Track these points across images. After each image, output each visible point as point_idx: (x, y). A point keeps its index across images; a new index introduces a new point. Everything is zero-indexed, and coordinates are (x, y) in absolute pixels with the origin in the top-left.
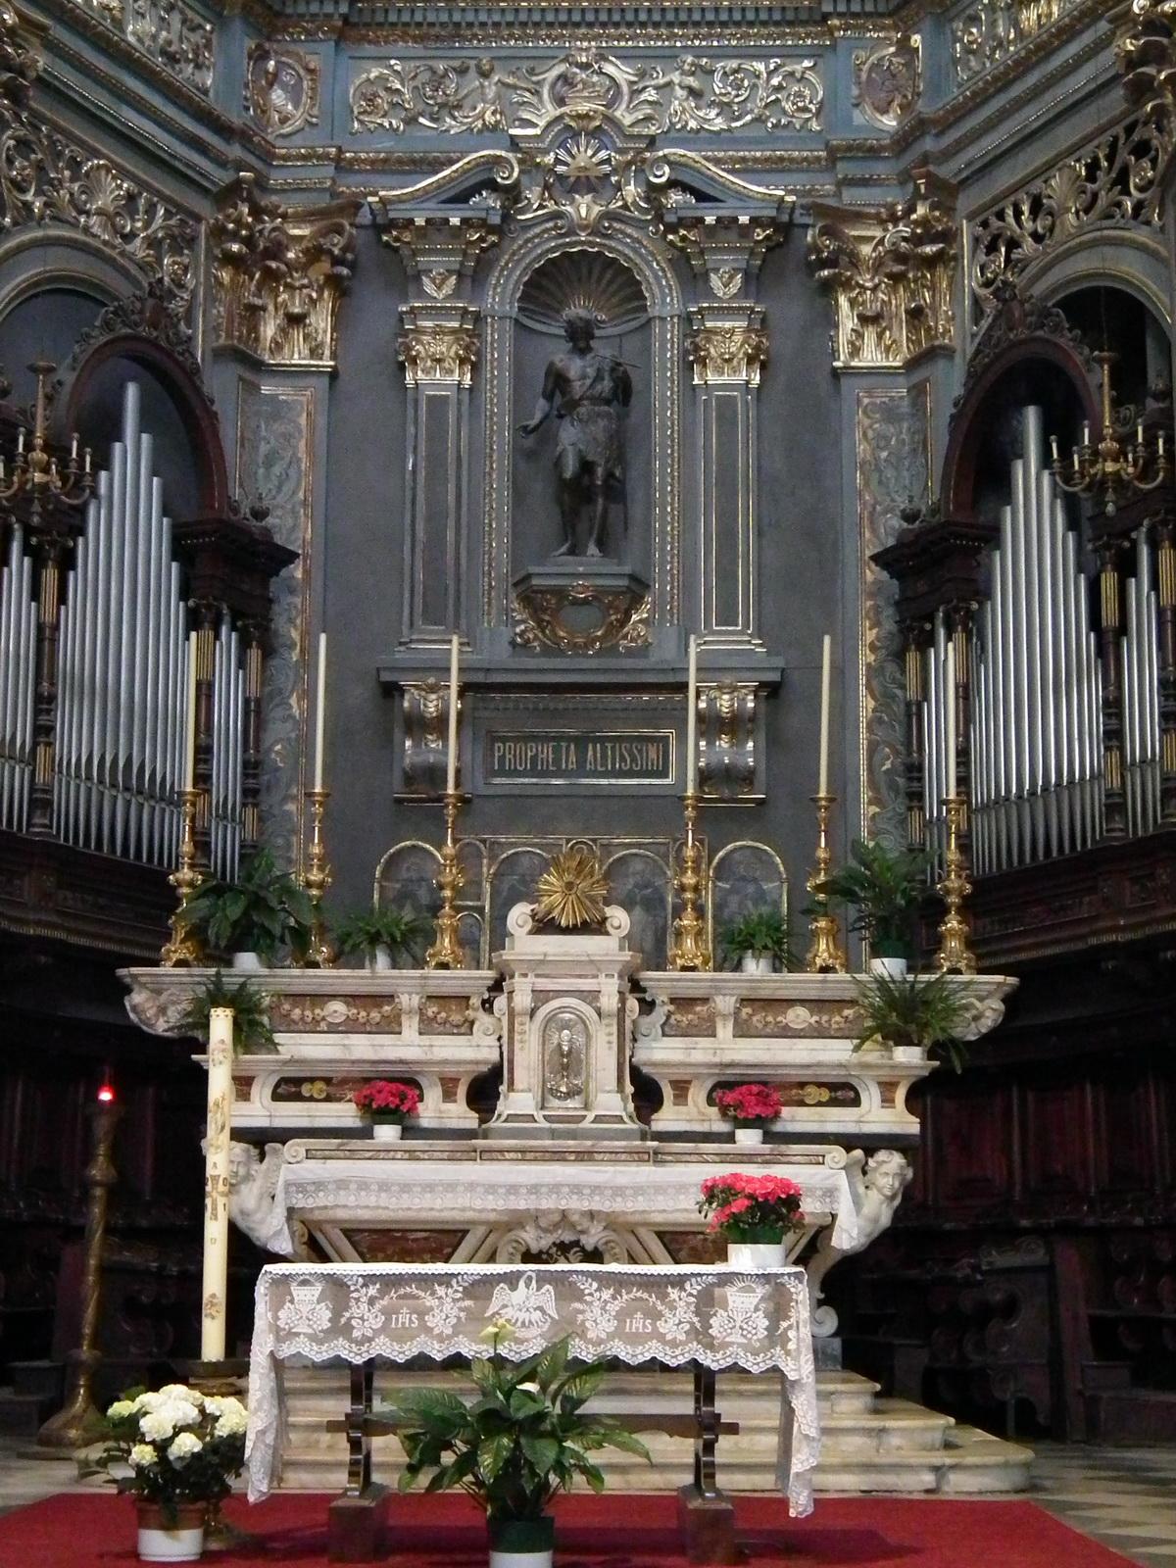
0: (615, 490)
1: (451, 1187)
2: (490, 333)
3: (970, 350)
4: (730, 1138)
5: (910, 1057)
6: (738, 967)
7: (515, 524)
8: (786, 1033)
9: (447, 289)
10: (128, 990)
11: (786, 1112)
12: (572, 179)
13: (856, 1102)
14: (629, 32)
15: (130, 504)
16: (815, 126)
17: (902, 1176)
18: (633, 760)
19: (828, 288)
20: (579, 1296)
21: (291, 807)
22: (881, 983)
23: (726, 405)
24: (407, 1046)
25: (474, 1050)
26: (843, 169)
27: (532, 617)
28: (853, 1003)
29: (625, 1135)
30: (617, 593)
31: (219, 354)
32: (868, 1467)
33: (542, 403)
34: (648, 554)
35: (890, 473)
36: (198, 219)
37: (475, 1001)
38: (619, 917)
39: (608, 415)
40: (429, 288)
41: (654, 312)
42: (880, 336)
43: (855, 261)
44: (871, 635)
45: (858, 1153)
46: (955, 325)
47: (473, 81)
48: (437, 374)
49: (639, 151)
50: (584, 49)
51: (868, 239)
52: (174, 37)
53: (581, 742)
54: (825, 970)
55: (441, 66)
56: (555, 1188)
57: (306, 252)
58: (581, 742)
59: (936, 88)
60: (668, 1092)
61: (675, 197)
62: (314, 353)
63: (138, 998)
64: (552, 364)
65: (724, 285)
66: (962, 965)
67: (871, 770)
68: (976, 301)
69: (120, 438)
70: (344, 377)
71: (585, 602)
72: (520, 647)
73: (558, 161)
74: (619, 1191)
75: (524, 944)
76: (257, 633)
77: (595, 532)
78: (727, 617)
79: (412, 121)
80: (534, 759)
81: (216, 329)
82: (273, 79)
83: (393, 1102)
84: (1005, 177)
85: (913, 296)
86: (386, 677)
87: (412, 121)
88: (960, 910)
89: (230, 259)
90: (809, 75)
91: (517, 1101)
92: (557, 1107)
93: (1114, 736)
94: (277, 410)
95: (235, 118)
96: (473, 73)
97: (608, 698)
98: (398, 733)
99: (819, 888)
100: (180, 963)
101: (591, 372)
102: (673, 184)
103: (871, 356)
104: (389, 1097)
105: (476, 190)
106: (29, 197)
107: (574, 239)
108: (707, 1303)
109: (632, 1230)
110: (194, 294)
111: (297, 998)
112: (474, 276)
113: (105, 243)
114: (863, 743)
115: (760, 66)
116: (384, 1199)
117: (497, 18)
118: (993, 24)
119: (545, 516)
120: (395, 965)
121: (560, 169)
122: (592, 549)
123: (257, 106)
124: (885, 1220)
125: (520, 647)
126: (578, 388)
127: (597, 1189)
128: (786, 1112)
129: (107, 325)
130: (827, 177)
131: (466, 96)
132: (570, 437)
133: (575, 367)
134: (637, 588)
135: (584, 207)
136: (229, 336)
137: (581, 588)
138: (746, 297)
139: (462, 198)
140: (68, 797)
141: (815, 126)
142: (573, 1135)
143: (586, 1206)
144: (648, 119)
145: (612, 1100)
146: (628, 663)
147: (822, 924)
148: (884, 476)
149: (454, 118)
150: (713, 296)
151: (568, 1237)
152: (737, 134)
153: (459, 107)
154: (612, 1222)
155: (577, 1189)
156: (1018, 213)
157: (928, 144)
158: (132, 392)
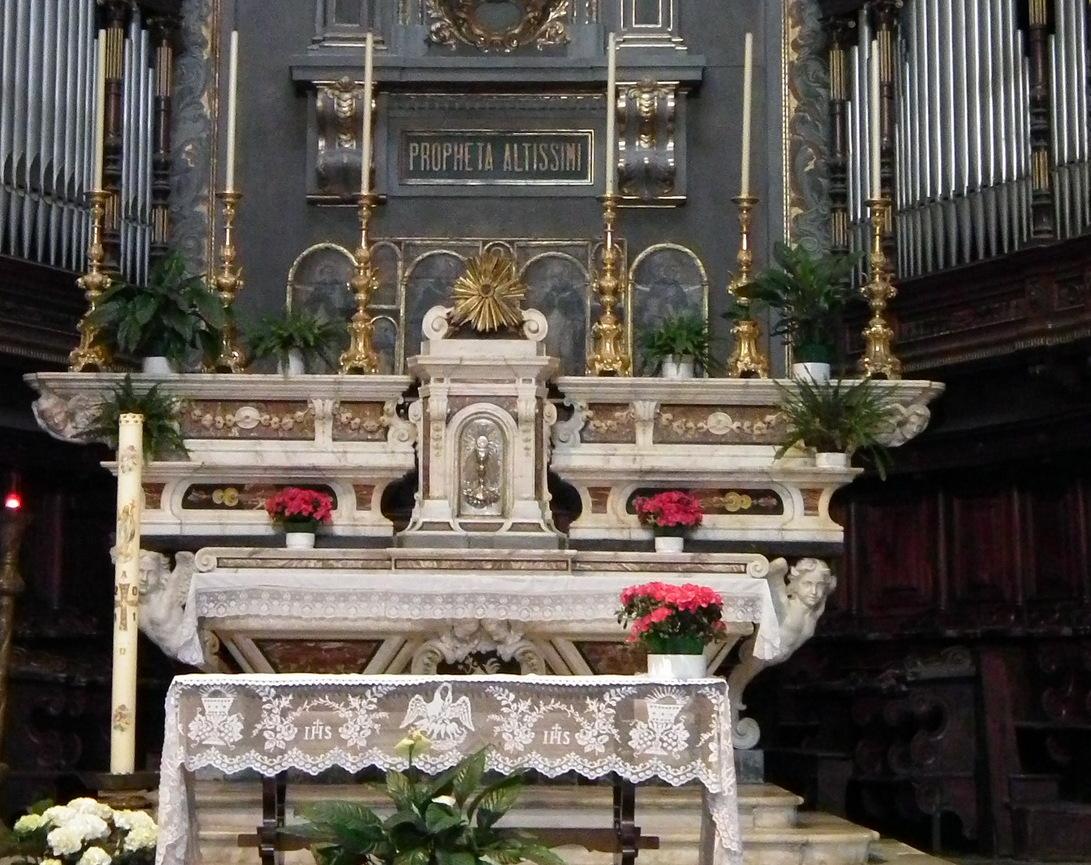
1: (365, 596)
4: (650, 546)
5: (833, 464)
6: (658, 372)
8: (707, 439)
10: (36, 396)
11: (707, 519)
13: (778, 509)
17: (826, 585)
18: (551, 160)
20: (496, 707)
22: (805, 388)
24: (321, 452)
25: (389, 456)
28: (775, 408)
37: (390, 407)
38: (536, 321)
44: (794, 33)
45: (781, 562)
53: (498, 142)
56: (471, 598)
58: (498, 142)
60: (586, 500)
63: (45, 403)
66: (887, 370)
67: (793, 170)
72: (436, 45)
74: (536, 600)
80: (450, 159)
83: (306, 509)
86: (299, 76)
88: (885, 314)
91: (433, 508)
93: (1041, 136)
98: (311, 133)
99: (740, 291)
104: (302, 504)
108: (626, 714)
111: (208, 403)
114: (786, 144)
116: (297, 609)
120: (308, 370)
124: (808, 630)
125: (436, 45)
127: (514, 598)
128: (707, 519)
143: (503, 615)
145: (529, 508)
146: (546, 62)
147: (744, 328)
151: (484, 647)
154: (529, 633)
155: (493, 598)
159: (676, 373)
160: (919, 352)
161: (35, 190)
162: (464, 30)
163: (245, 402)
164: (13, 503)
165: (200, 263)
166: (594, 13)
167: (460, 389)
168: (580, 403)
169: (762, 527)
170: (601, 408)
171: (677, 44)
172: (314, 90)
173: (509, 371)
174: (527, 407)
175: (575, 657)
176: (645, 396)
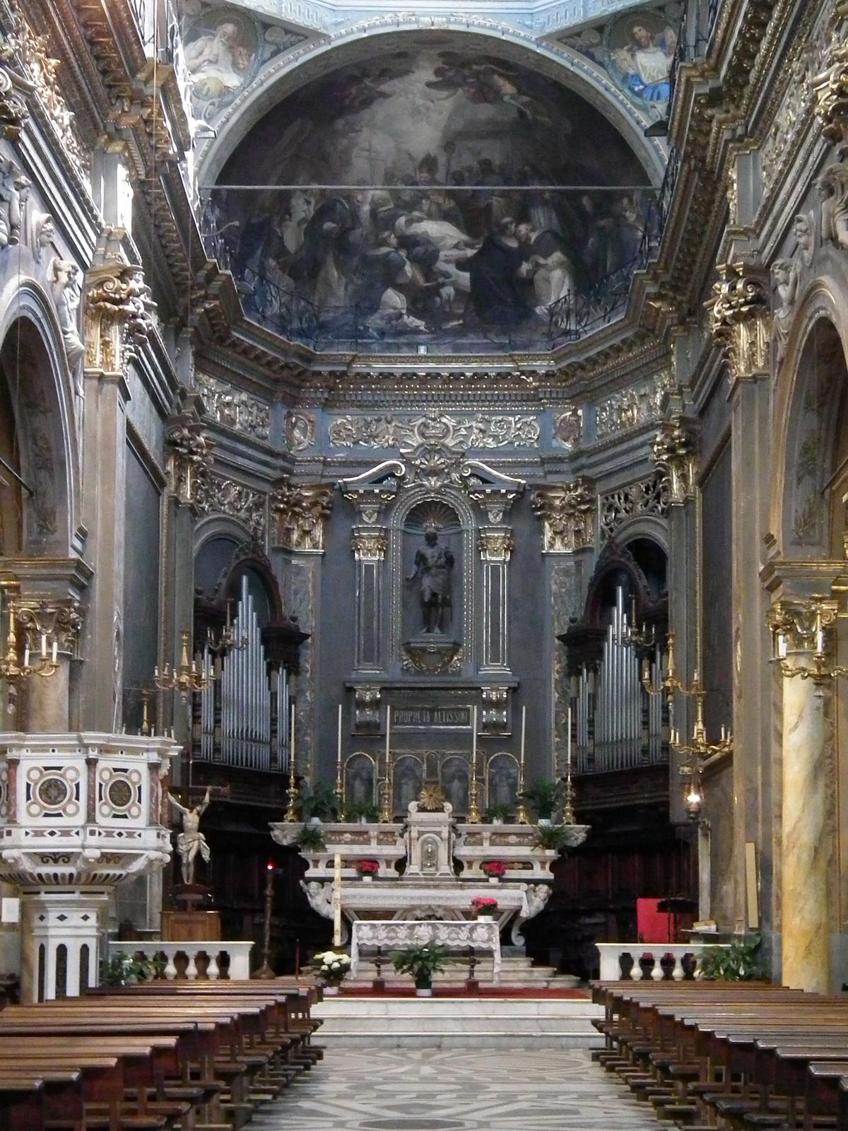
0: (447, 603)
1: (391, 897)
2: (392, 537)
3: (600, 551)
4: (487, 880)
5: (551, 853)
6: (491, 822)
7: (403, 620)
8: (508, 844)
9: (373, 519)
10: (272, 830)
11: (507, 871)
13: (532, 868)
14: (453, 404)
15: (246, 625)
16: (536, 445)
17: (547, 892)
18: (454, 718)
19: (540, 518)
20: (438, 929)
21: (308, 738)
22: (542, 829)
23: (495, 570)
24: (373, 849)
25: (397, 850)
26: (547, 467)
28: (531, 834)
29: (450, 880)
30: (448, 650)
31: (275, 550)
32: (525, 981)
33: (414, 567)
35: (566, 598)
36: (265, 493)
37: (397, 834)
38: (448, 806)
39: (443, 573)
40: (365, 519)
41: (464, 527)
42: (563, 540)
43: (552, 507)
44: (557, 667)
45: (532, 885)
46: (593, 539)
47: (383, 425)
48: (368, 556)
49: (457, 459)
50: (433, 412)
51: (559, 497)
52: (254, 418)
53: (432, 711)
54: (522, 823)
55: (369, 419)
56: (427, 898)
57: (311, 503)
58: (432, 711)
59: (588, 436)
60: (466, 865)
61: (473, 481)
62: (315, 546)
63: (277, 832)
64: (419, 552)
65: (495, 517)
66: (571, 821)
67: (556, 723)
68: (603, 531)
69: (241, 599)
70: (327, 557)
72: (406, 671)
73: (421, 463)
74: (448, 898)
75: (414, 815)
76: (294, 668)
78: (495, 659)
79: (356, 443)
80: (412, 718)
81: (273, 539)
82: (294, 425)
83: (370, 869)
84: (614, 482)
85: (577, 524)
86: (348, 685)
87: (356, 443)
88: (571, 802)
89: (278, 510)
90: (533, 423)
91: (413, 868)
92: (427, 870)
93: (646, 724)
94: (299, 571)
95: (279, 449)
96: (383, 421)
97: (443, 692)
98: (353, 707)
99: (520, 795)
100: (291, 821)
101: (436, 555)
102: (471, 475)
103: (559, 548)
104: (367, 867)
105: (385, 478)
106: (203, 505)
108: (473, 929)
109: (453, 911)
110: (264, 526)
111: (334, 833)
113: (232, 515)
114: (553, 711)
115: (511, 419)
116: (369, 901)
117: (394, 398)
118: (611, 414)
119: (417, 612)
120: (368, 822)
121: (422, 466)
122: (437, 630)
123: (288, 438)
124: (542, 907)
125: (406, 671)
126: (431, 562)
127: (440, 898)
128: (507, 871)
129: (237, 557)
130: (541, 469)
132: (427, 583)
133: (429, 552)
134: (456, 647)
135: (433, 482)
136: (279, 543)
137: (432, 648)
138: (504, 523)
139: (380, 481)
140: (227, 746)
141: (536, 445)
142: (432, 880)
143: (437, 903)
144: (461, 442)
145: (446, 868)
146: (452, 679)
147: (521, 807)
148: (563, 604)
150: (489, 523)
151: (430, 913)
152: (502, 449)
153: (377, 437)
154: (446, 909)
155: (434, 898)
156: (619, 499)
157: (584, 461)
158: (245, 579)
159: (497, 823)
160: (602, 801)
161: (247, 739)
163: (346, 832)
164: (270, 867)
165: (307, 760)
167: (422, 829)
168: (464, 833)
169: (526, 874)
170: (471, 834)
171: (508, 671)
172: (355, 691)
173: (439, 823)
174: (445, 835)
175: (461, 916)
176: (486, 830)
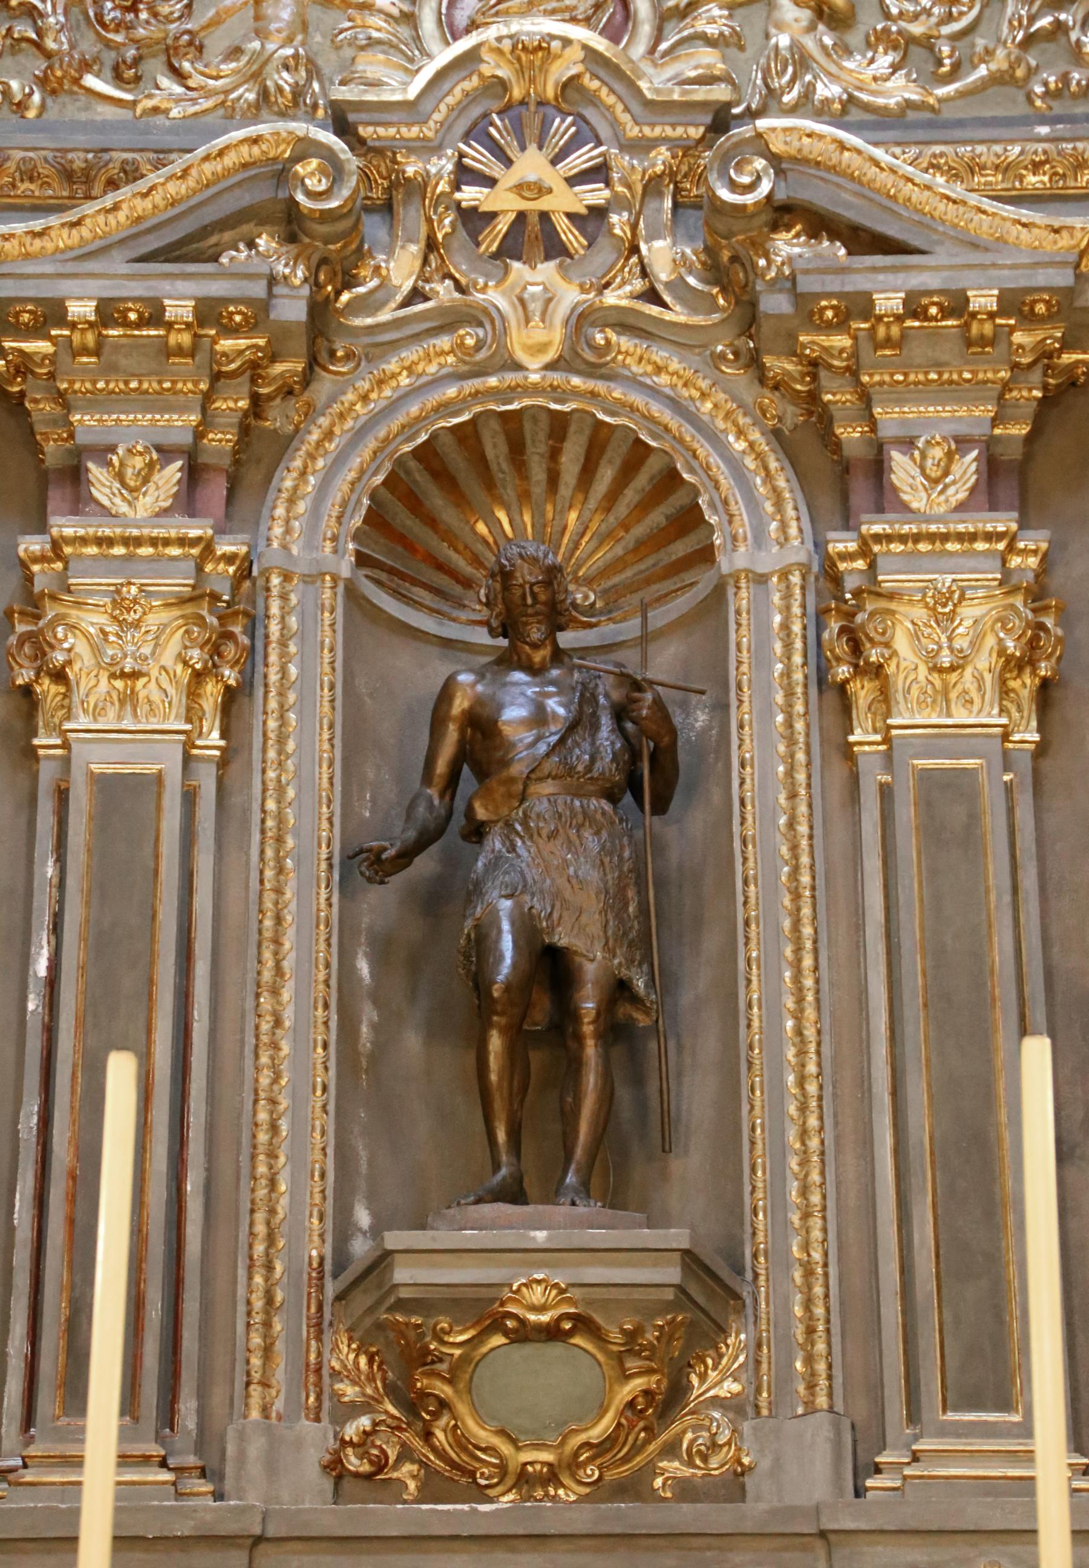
12: (503, 225)
27: (392, 1391)
34: (732, 1208)
61: (788, 246)
65: (932, 485)
71: (552, 1333)
77: (589, 1006)
105: (240, 222)
107: (511, 378)
112: (230, 474)
121: (470, 195)
131: (215, 22)
137: (536, 1300)
149: (179, 75)
152: (947, 113)
162: (440, 1434)
166: (823, 1382)
